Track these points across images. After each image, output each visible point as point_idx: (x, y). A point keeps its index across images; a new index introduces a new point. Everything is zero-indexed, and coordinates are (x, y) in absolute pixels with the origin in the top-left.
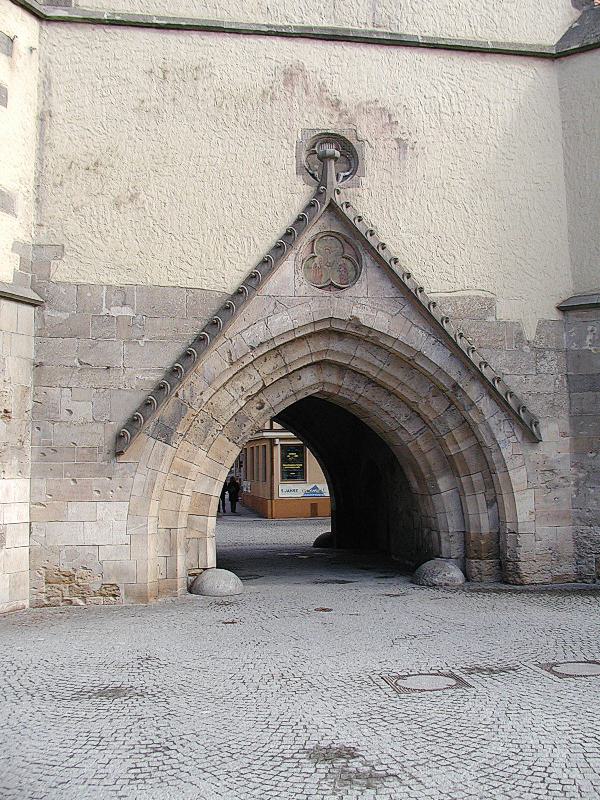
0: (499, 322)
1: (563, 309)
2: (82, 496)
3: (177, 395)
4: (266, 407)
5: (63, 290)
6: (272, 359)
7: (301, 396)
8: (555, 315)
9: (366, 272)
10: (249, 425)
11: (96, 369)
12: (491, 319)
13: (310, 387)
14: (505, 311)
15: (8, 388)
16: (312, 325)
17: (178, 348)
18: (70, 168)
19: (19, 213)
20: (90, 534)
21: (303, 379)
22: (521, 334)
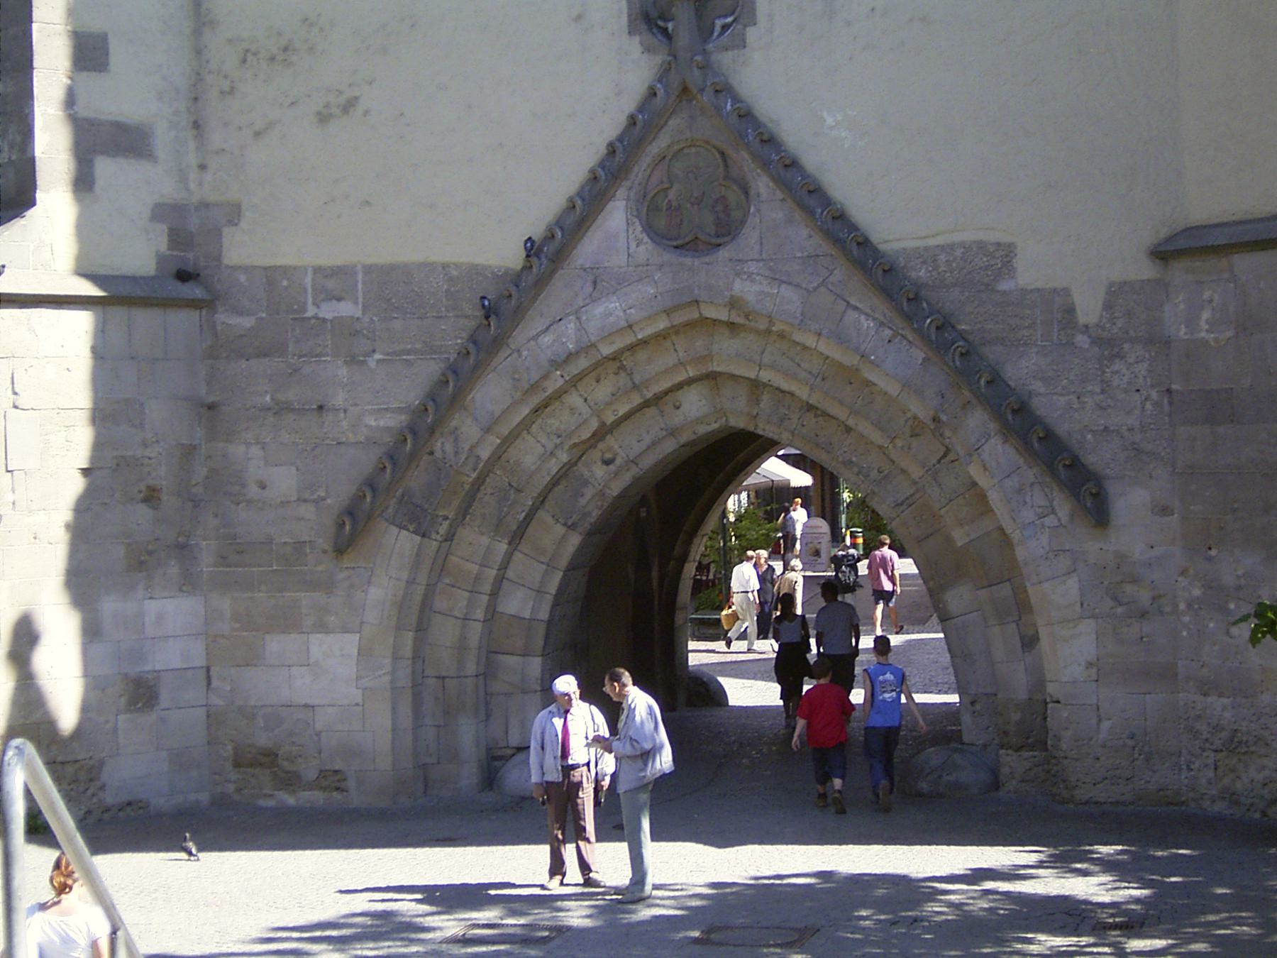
0: (1024, 292)
1: (1163, 254)
2: (287, 621)
3: (431, 453)
4: (619, 461)
5: (243, 278)
6: (612, 377)
7: (686, 437)
8: (1145, 270)
9: (758, 210)
10: (589, 492)
11: (301, 411)
12: (1004, 286)
13: (699, 421)
14: (1030, 273)
15: (152, 452)
16: (664, 316)
17: (430, 369)
18: (244, 61)
19: (161, 153)
20: (301, 687)
21: (685, 407)
22: (1071, 310)
